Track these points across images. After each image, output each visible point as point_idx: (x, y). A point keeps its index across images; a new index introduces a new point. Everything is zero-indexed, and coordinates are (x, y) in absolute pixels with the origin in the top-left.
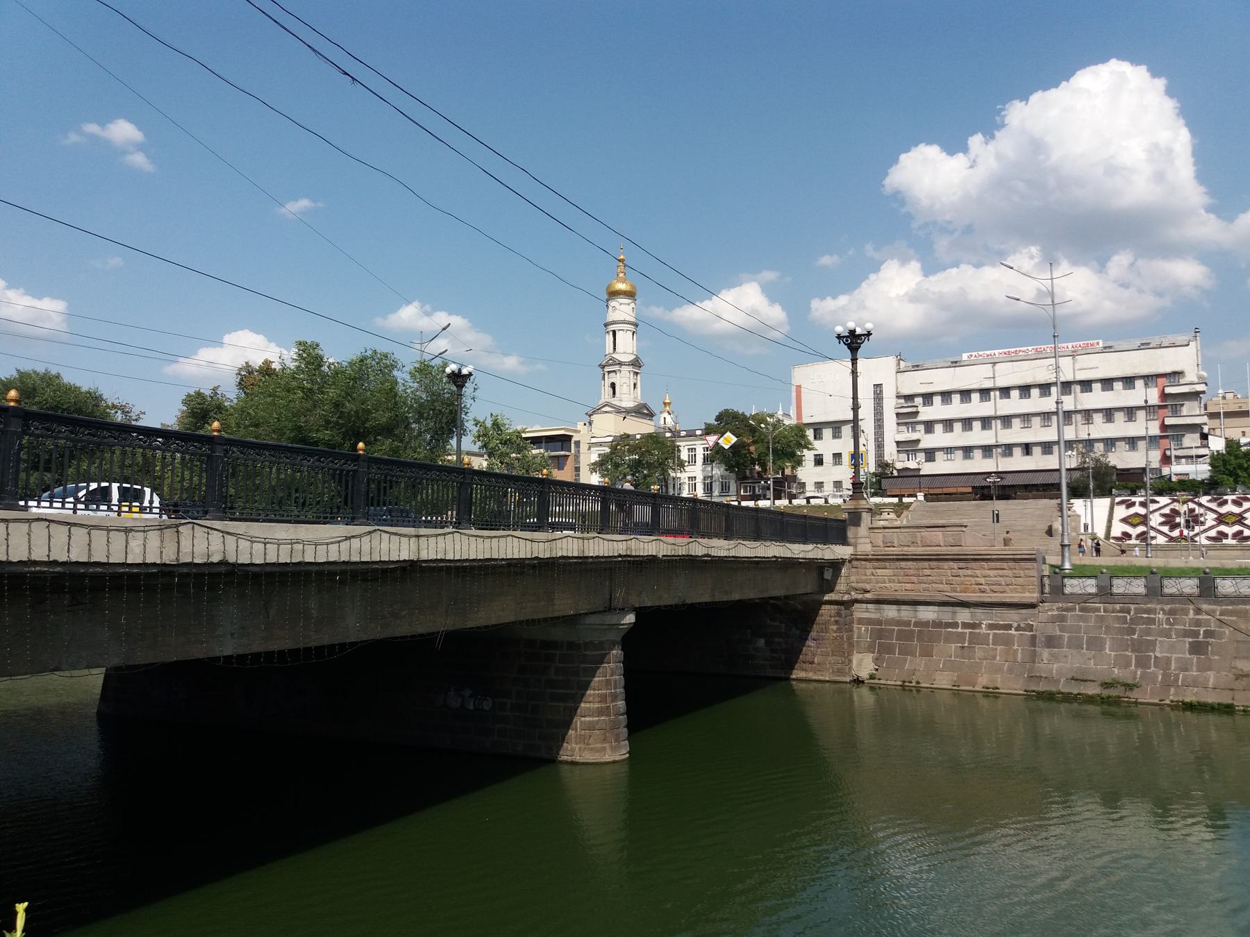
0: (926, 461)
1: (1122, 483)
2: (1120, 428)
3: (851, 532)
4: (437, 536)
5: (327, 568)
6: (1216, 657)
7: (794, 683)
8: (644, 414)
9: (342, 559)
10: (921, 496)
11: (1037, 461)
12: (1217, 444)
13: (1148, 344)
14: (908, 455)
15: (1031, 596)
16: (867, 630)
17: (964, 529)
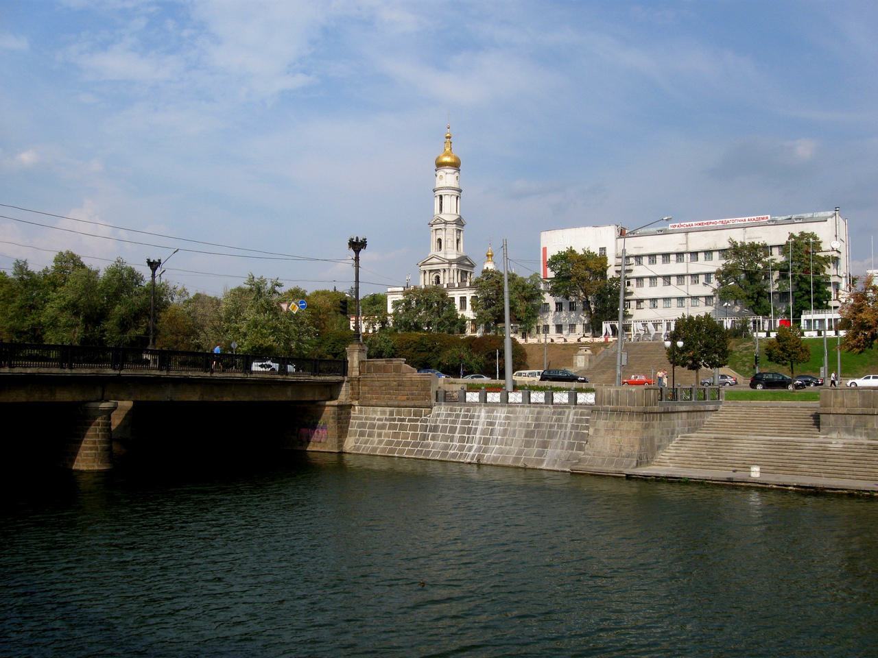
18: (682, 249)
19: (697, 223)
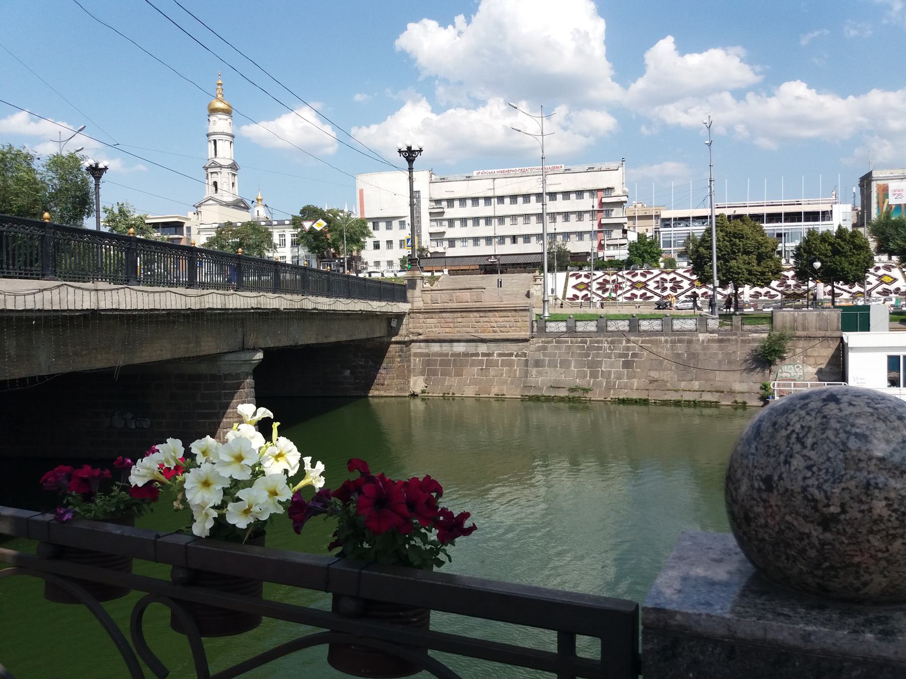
0: (449, 247)
1: (574, 263)
2: (573, 225)
3: (409, 294)
4: (111, 290)
5: (24, 314)
6: (638, 370)
7: (370, 399)
8: (241, 207)
9: (37, 308)
10: (446, 272)
11: (521, 248)
12: (632, 237)
13: (593, 168)
14: (437, 243)
15: (525, 334)
16: (420, 361)
17: (483, 290)
18: (490, 194)
19: (498, 170)
